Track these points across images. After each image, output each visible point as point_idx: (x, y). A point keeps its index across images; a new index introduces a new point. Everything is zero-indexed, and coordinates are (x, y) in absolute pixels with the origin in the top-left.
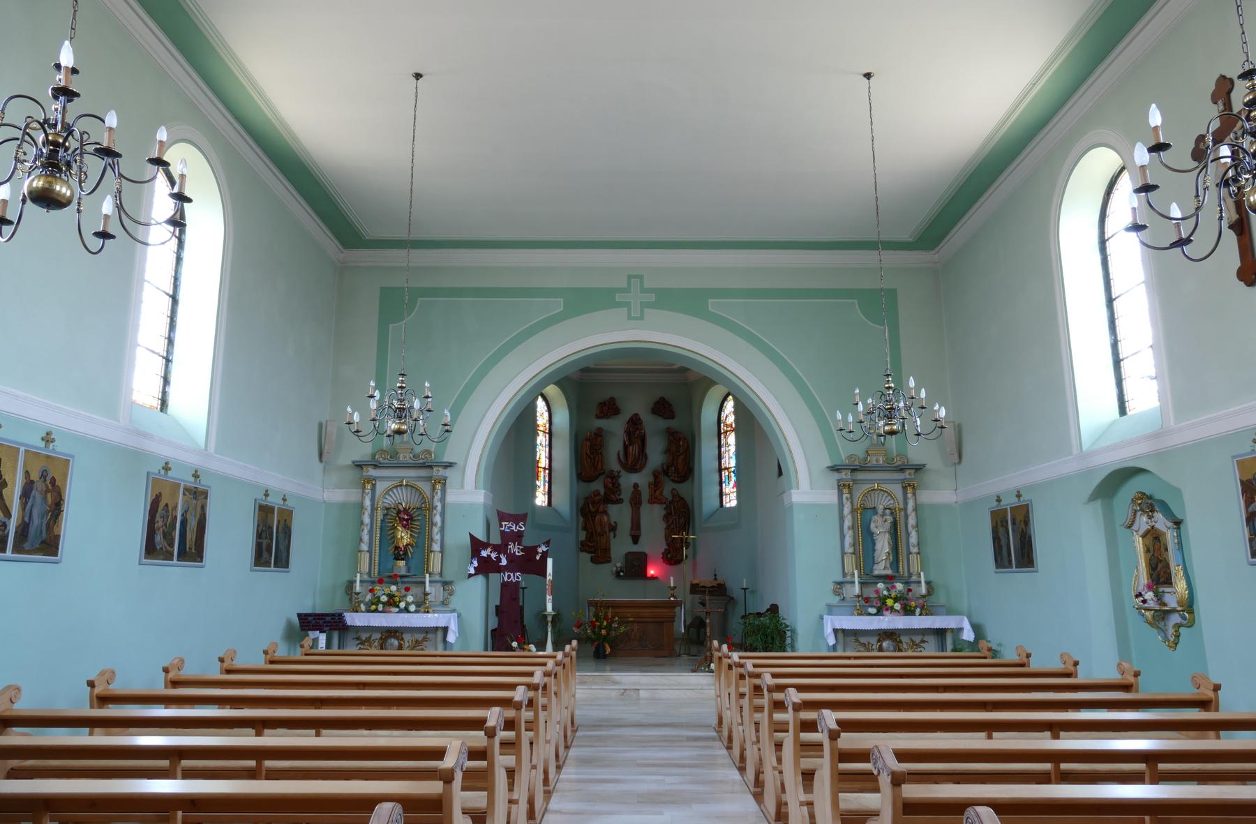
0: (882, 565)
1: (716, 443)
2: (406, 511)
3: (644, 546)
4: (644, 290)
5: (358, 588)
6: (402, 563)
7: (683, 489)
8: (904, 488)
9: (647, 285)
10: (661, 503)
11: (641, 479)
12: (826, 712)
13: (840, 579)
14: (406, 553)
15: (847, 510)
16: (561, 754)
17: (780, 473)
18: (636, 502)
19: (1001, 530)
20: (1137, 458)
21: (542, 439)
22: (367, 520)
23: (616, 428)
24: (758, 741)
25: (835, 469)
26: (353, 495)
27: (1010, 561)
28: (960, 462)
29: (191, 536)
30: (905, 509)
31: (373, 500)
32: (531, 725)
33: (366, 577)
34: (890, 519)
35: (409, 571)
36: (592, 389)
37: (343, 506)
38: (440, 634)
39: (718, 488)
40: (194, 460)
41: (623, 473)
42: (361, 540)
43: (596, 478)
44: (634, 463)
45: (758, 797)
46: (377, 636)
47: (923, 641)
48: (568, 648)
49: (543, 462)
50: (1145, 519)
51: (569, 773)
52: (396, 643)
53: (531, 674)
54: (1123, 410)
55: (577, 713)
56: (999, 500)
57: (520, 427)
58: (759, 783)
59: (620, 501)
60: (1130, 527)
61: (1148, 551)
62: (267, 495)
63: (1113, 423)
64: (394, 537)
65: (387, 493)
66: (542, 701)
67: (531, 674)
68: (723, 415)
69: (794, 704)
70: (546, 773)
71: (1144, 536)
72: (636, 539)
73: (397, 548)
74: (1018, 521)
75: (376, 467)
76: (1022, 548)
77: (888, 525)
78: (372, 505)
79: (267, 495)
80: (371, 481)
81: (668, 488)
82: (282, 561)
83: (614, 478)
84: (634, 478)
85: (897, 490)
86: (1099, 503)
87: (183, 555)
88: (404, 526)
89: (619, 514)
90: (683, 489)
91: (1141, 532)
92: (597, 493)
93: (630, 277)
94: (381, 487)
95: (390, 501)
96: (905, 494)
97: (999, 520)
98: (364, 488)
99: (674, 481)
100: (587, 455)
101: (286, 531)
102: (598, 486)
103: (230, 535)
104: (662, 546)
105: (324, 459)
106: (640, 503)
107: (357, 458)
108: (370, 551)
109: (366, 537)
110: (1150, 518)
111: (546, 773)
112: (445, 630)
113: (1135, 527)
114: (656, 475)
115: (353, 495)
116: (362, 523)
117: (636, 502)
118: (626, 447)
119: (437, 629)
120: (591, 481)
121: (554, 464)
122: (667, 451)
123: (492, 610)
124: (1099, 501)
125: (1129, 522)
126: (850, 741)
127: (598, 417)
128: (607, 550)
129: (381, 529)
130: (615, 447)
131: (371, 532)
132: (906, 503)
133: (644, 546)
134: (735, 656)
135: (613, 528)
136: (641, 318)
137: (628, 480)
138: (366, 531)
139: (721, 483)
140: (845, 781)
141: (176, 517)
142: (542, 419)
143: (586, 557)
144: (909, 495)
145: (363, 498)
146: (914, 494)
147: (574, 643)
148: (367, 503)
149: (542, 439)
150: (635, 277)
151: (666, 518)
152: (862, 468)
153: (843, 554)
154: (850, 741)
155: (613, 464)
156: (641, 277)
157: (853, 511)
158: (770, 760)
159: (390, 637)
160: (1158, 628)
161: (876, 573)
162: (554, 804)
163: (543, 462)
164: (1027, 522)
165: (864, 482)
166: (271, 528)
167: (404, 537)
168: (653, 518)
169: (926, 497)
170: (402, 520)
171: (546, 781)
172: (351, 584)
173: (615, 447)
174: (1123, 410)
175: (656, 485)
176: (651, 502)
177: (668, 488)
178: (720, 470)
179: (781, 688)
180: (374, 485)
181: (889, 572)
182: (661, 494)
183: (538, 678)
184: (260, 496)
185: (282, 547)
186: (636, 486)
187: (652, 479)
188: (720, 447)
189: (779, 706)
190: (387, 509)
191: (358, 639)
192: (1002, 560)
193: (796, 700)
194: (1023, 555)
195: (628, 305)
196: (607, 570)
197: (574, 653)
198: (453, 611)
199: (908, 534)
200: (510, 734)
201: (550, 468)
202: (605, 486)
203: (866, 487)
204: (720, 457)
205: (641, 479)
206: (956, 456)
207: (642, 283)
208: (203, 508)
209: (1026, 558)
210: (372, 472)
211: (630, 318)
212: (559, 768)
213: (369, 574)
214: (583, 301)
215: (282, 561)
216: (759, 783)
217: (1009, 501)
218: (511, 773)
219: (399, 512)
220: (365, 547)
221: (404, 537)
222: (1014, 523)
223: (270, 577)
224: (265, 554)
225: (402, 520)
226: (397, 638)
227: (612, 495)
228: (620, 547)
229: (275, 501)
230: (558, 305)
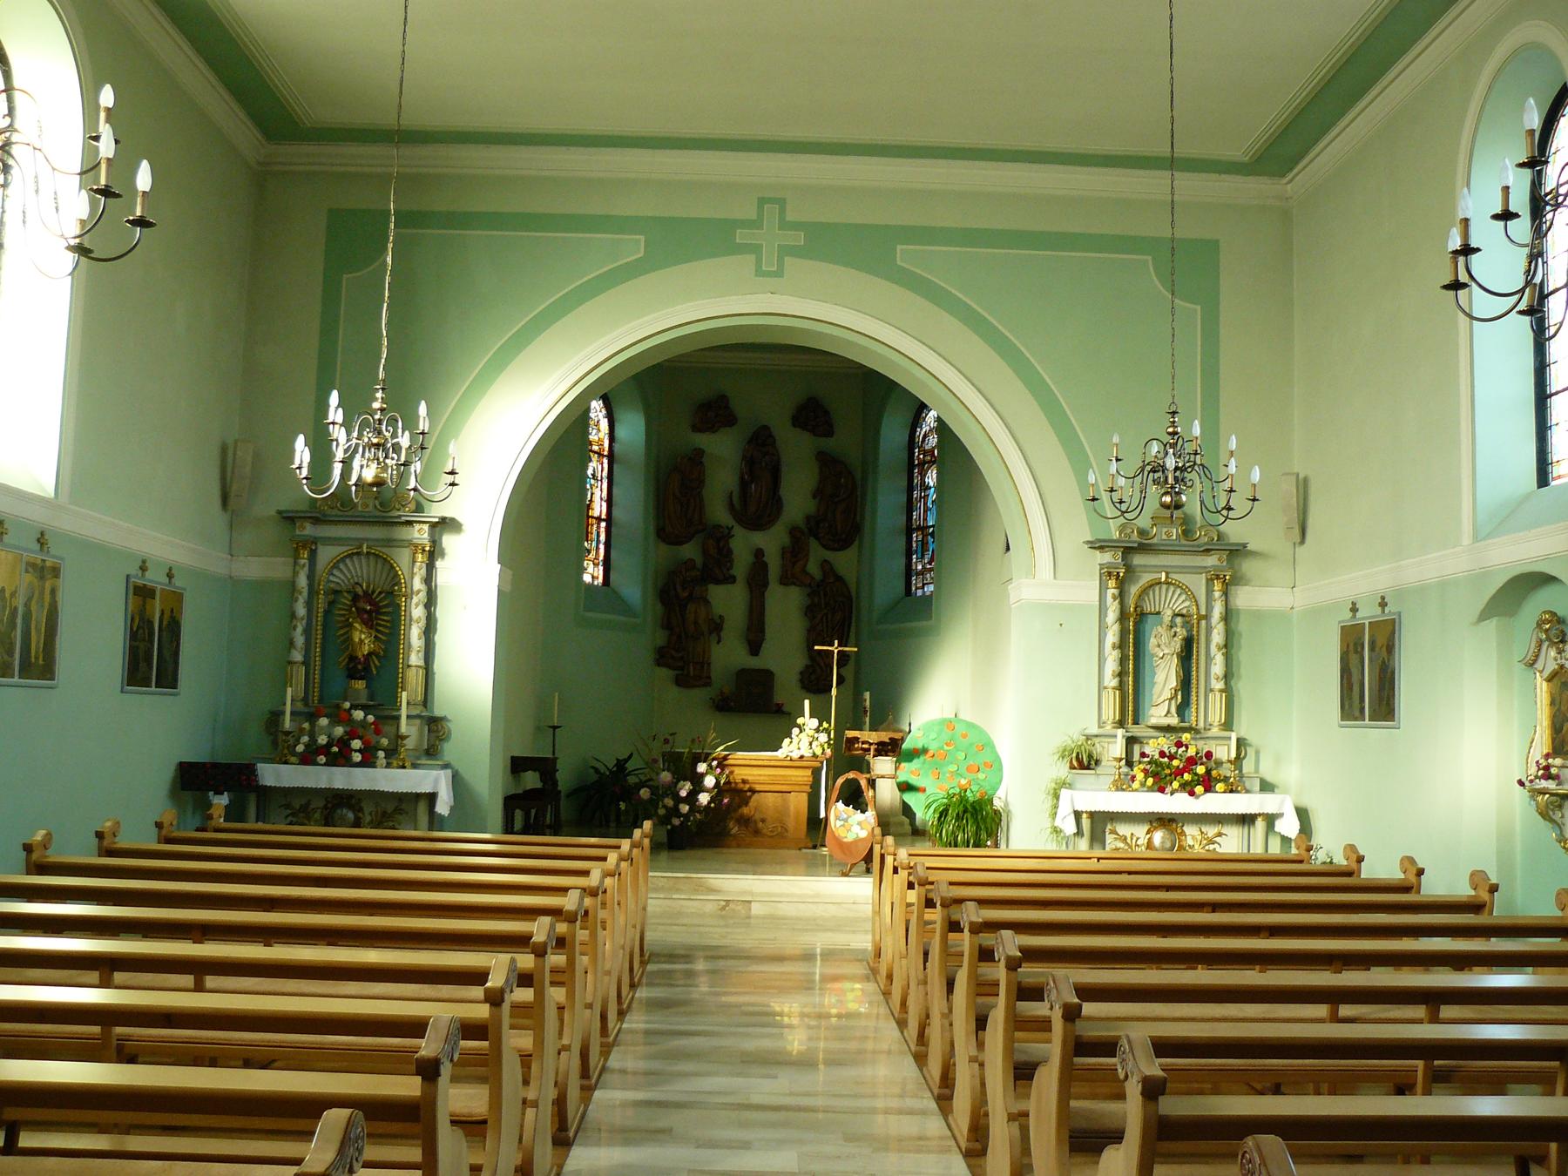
0: (1164, 709)
1: (905, 483)
2: (368, 596)
3: (770, 658)
4: (784, 225)
5: (287, 723)
6: (360, 685)
7: (844, 562)
8: (1210, 581)
9: (790, 217)
10: (801, 584)
11: (771, 541)
12: (1007, 934)
13: (1094, 730)
14: (367, 668)
15: (1112, 615)
16: (624, 993)
17: (1008, 549)
18: (758, 581)
19: (1354, 658)
20: (1546, 558)
21: (597, 467)
22: (301, 611)
23: (723, 452)
24: (925, 983)
25: (1100, 546)
26: (274, 568)
27: (1362, 710)
28: (1303, 541)
29: (36, 641)
30: (1207, 617)
31: (311, 577)
32: (562, 977)
33: (300, 706)
34: (1182, 633)
35: (371, 697)
36: (685, 393)
37: (261, 586)
38: (422, 808)
39: (903, 561)
40: (39, 516)
41: (738, 531)
42: (291, 644)
43: (688, 539)
44: (757, 506)
45: (920, 1059)
46: (318, 803)
47: (1220, 835)
48: (637, 833)
49: (599, 508)
50: (1553, 653)
51: (636, 1022)
52: (351, 815)
53: (586, 873)
54: (1543, 478)
55: (649, 936)
56: (1354, 609)
57: (562, 448)
58: (922, 1038)
59: (732, 580)
60: (1532, 664)
61: (1552, 703)
62: (143, 569)
63: (1528, 497)
64: (349, 639)
65: (336, 566)
66: (582, 935)
67: (605, 859)
68: (921, 433)
69: (971, 924)
70: (604, 1018)
71: (1549, 680)
72: (755, 648)
73: (353, 658)
74: (1379, 644)
75: (316, 521)
76: (1381, 688)
77: (1177, 644)
78: (311, 586)
79: (143, 569)
80: (311, 545)
81: (816, 554)
82: (168, 679)
83: (719, 542)
84: (759, 539)
85: (1198, 584)
86: (1492, 625)
87: (27, 670)
88: (364, 623)
89: (728, 601)
90: (844, 562)
91: (1546, 674)
92: (690, 564)
93: (762, 201)
94: (326, 554)
95: (340, 578)
96: (1209, 592)
97: (1351, 641)
98: (296, 557)
99: (825, 547)
100: (674, 491)
101: (173, 628)
102: (690, 551)
103: (93, 639)
104: (798, 662)
105: (232, 501)
106: (765, 585)
107: (284, 506)
108: (306, 663)
109: (300, 640)
110: (1560, 652)
111: (604, 1018)
112: (432, 798)
113: (1539, 665)
114: (794, 532)
115: (274, 568)
116: (293, 616)
117: (758, 581)
118: (744, 485)
119: (418, 796)
120: (681, 543)
121: (616, 513)
122: (818, 493)
123: (1004, 823)
124: (1494, 620)
125: (1530, 656)
126: (1031, 972)
127: (696, 429)
128: (704, 664)
129: (325, 626)
130: (722, 481)
131: (307, 632)
132: (1209, 608)
133: (770, 658)
134: (903, 853)
135: (717, 626)
136: (779, 273)
137: (743, 543)
138: (300, 629)
139: (909, 553)
140: (1018, 1024)
141: (16, 609)
142: (599, 432)
143: (665, 673)
144: (1217, 594)
145: (295, 574)
146: (1226, 594)
147: (647, 825)
148: (302, 581)
149: (597, 467)
150: (771, 200)
151: (810, 611)
152: (1144, 548)
153: (1101, 688)
154: (1031, 972)
155: (718, 512)
156: (782, 203)
157: (1123, 617)
158: (938, 1005)
159: (340, 805)
160: (1552, 820)
161: (1153, 721)
162: (614, 1061)
163: (599, 508)
164: (1390, 648)
165: (1147, 568)
166: (151, 623)
167: (364, 641)
168: (786, 609)
169: (1244, 598)
170: (360, 611)
171: (604, 1031)
172: (276, 716)
173: (722, 481)
174: (1543, 478)
175: (794, 552)
176: (785, 580)
177: (816, 554)
178: (909, 530)
179: (959, 901)
180: (313, 554)
181: (1174, 720)
182: (804, 571)
183: (594, 880)
184: (134, 570)
185: (167, 654)
186: (759, 553)
187: (787, 540)
188: (910, 488)
189: (954, 926)
190: (336, 592)
191: (288, 806)
192: (1350, 708)
193: (975, 919)
194: (1381, 699)
195: (755, 249)
196: (698, 695)
197: (646, 841)
198: (446, 766)
199: (1209, 659)
200: (525, 995)
201: (609, 519)
202: (705, 552)
203: (1146, 578)
204: (910, 508)
205: (771, 541)
206: (1297, 531)
207: (782, 211)
208: (53, 592)
209: (1384, 707)
210: (309, 530)
211: (759, 272)
212: (633, 986)
213: (305, 700)
214: (681, 240)
215: (168, 679)
216: (947, 1080)
217: (1368, 613)
218: (526, 1059)
219: (356, 598)
220: (298, 656)
221: (364, 641)
222: (1372, 649)
223: (149, 704)
224: (143, 665)
225: (360, 611)
226: (351, 807)
227: (717, 568)
228: (728, 655)
229: (155, 578)
230: (634, 247)
